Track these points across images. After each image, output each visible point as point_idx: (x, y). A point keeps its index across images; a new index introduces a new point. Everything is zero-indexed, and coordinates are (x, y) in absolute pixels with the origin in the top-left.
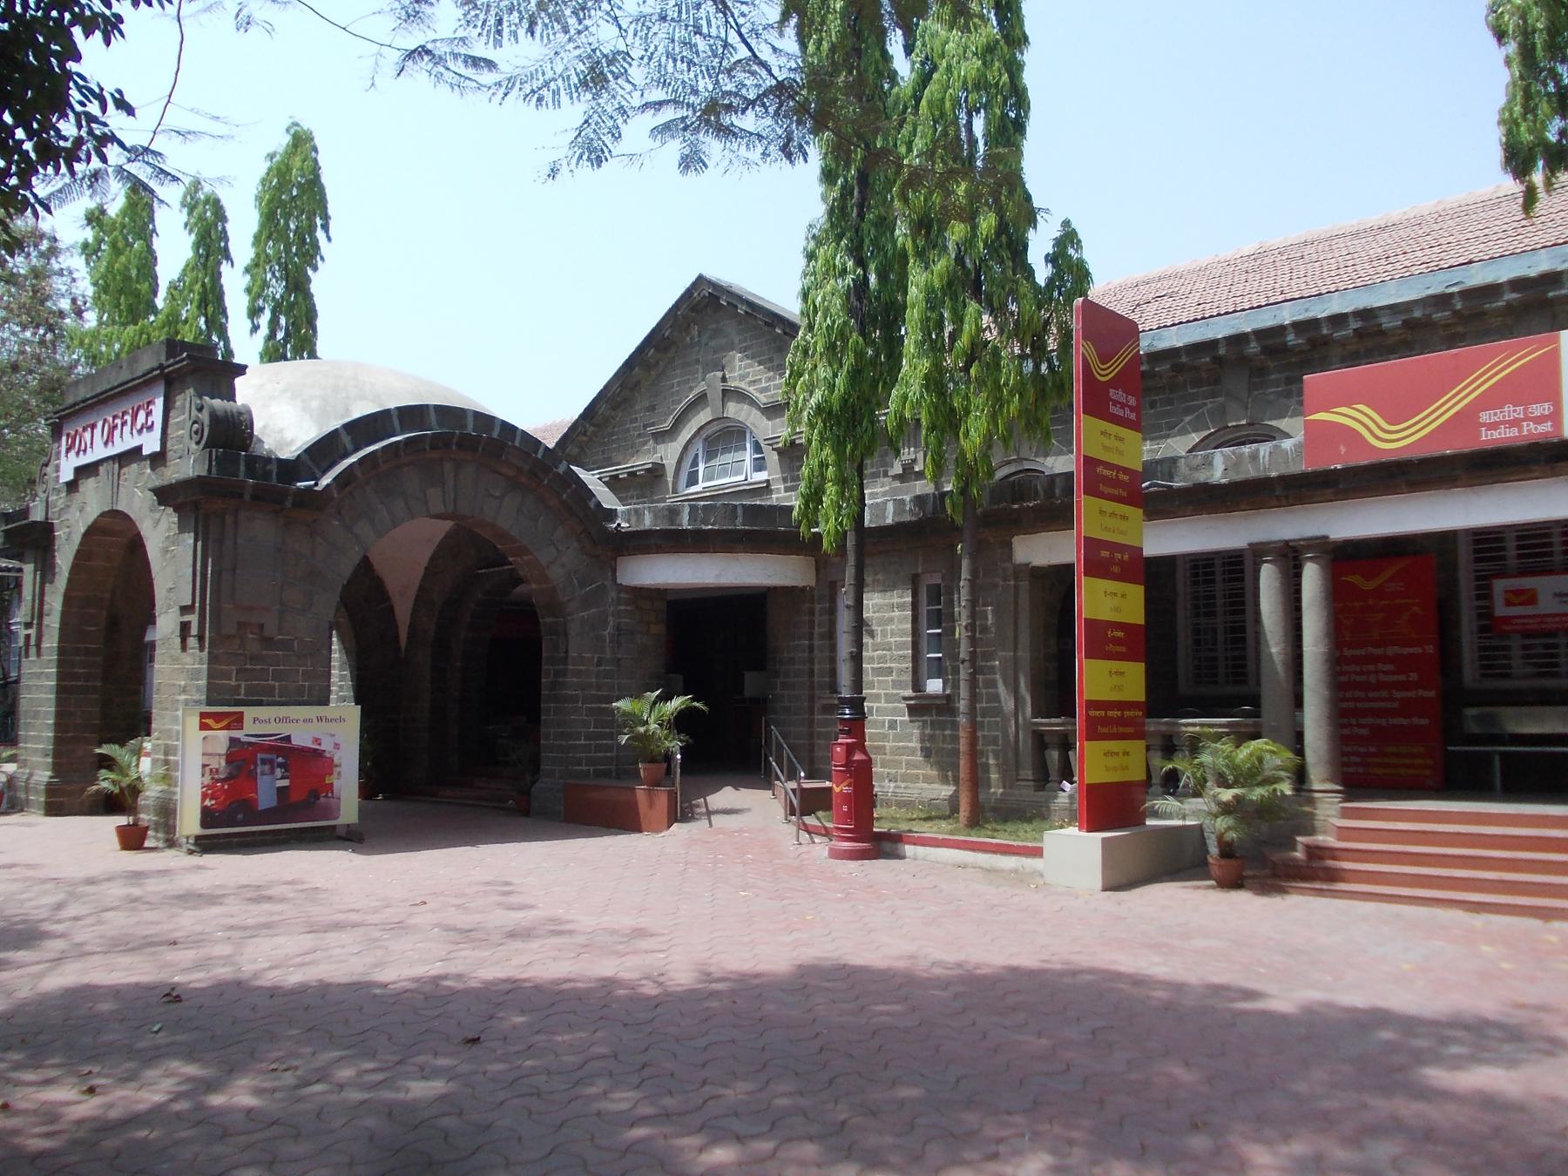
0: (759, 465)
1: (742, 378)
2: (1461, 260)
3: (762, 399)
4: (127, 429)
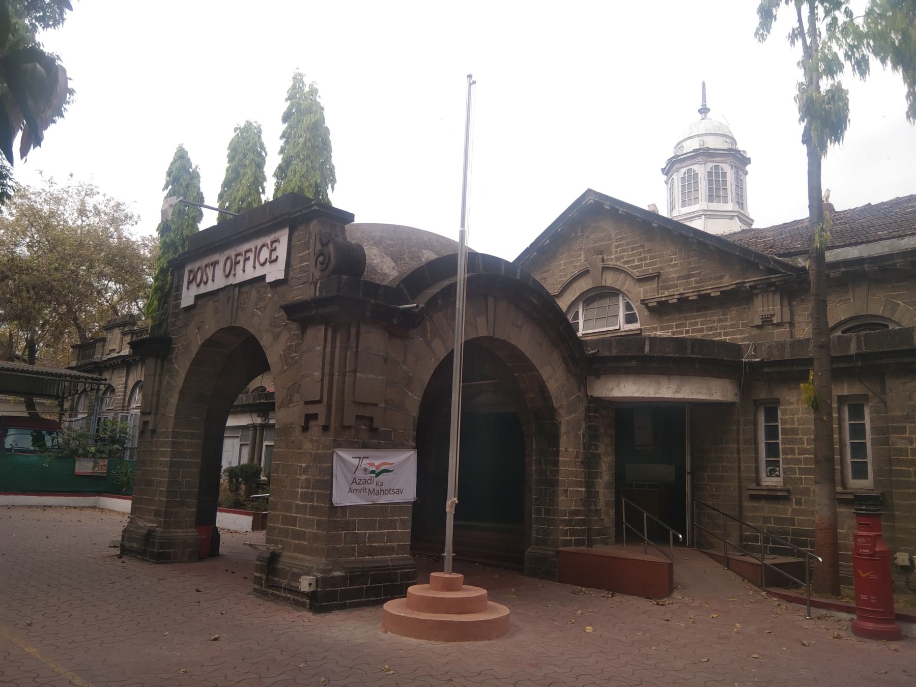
0: (630, 319)
1: (618, 259)
2: (853, 241)
3: (636, 273)
4: (250, 264)
